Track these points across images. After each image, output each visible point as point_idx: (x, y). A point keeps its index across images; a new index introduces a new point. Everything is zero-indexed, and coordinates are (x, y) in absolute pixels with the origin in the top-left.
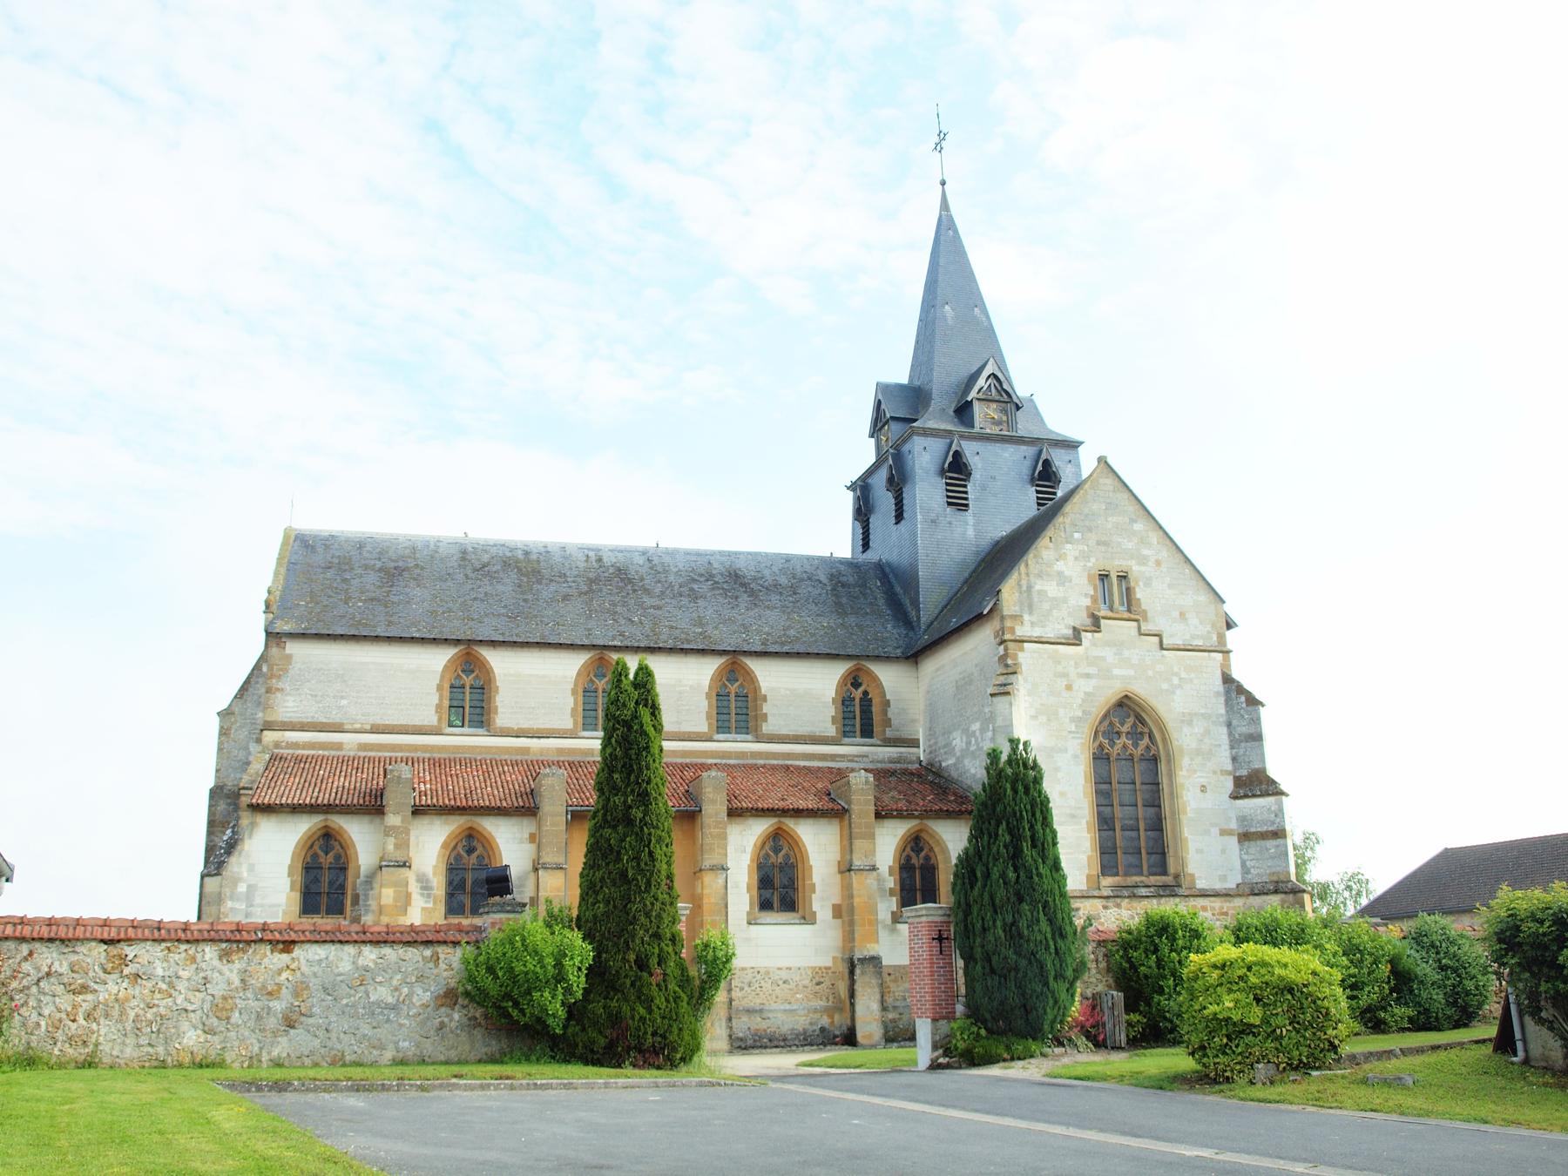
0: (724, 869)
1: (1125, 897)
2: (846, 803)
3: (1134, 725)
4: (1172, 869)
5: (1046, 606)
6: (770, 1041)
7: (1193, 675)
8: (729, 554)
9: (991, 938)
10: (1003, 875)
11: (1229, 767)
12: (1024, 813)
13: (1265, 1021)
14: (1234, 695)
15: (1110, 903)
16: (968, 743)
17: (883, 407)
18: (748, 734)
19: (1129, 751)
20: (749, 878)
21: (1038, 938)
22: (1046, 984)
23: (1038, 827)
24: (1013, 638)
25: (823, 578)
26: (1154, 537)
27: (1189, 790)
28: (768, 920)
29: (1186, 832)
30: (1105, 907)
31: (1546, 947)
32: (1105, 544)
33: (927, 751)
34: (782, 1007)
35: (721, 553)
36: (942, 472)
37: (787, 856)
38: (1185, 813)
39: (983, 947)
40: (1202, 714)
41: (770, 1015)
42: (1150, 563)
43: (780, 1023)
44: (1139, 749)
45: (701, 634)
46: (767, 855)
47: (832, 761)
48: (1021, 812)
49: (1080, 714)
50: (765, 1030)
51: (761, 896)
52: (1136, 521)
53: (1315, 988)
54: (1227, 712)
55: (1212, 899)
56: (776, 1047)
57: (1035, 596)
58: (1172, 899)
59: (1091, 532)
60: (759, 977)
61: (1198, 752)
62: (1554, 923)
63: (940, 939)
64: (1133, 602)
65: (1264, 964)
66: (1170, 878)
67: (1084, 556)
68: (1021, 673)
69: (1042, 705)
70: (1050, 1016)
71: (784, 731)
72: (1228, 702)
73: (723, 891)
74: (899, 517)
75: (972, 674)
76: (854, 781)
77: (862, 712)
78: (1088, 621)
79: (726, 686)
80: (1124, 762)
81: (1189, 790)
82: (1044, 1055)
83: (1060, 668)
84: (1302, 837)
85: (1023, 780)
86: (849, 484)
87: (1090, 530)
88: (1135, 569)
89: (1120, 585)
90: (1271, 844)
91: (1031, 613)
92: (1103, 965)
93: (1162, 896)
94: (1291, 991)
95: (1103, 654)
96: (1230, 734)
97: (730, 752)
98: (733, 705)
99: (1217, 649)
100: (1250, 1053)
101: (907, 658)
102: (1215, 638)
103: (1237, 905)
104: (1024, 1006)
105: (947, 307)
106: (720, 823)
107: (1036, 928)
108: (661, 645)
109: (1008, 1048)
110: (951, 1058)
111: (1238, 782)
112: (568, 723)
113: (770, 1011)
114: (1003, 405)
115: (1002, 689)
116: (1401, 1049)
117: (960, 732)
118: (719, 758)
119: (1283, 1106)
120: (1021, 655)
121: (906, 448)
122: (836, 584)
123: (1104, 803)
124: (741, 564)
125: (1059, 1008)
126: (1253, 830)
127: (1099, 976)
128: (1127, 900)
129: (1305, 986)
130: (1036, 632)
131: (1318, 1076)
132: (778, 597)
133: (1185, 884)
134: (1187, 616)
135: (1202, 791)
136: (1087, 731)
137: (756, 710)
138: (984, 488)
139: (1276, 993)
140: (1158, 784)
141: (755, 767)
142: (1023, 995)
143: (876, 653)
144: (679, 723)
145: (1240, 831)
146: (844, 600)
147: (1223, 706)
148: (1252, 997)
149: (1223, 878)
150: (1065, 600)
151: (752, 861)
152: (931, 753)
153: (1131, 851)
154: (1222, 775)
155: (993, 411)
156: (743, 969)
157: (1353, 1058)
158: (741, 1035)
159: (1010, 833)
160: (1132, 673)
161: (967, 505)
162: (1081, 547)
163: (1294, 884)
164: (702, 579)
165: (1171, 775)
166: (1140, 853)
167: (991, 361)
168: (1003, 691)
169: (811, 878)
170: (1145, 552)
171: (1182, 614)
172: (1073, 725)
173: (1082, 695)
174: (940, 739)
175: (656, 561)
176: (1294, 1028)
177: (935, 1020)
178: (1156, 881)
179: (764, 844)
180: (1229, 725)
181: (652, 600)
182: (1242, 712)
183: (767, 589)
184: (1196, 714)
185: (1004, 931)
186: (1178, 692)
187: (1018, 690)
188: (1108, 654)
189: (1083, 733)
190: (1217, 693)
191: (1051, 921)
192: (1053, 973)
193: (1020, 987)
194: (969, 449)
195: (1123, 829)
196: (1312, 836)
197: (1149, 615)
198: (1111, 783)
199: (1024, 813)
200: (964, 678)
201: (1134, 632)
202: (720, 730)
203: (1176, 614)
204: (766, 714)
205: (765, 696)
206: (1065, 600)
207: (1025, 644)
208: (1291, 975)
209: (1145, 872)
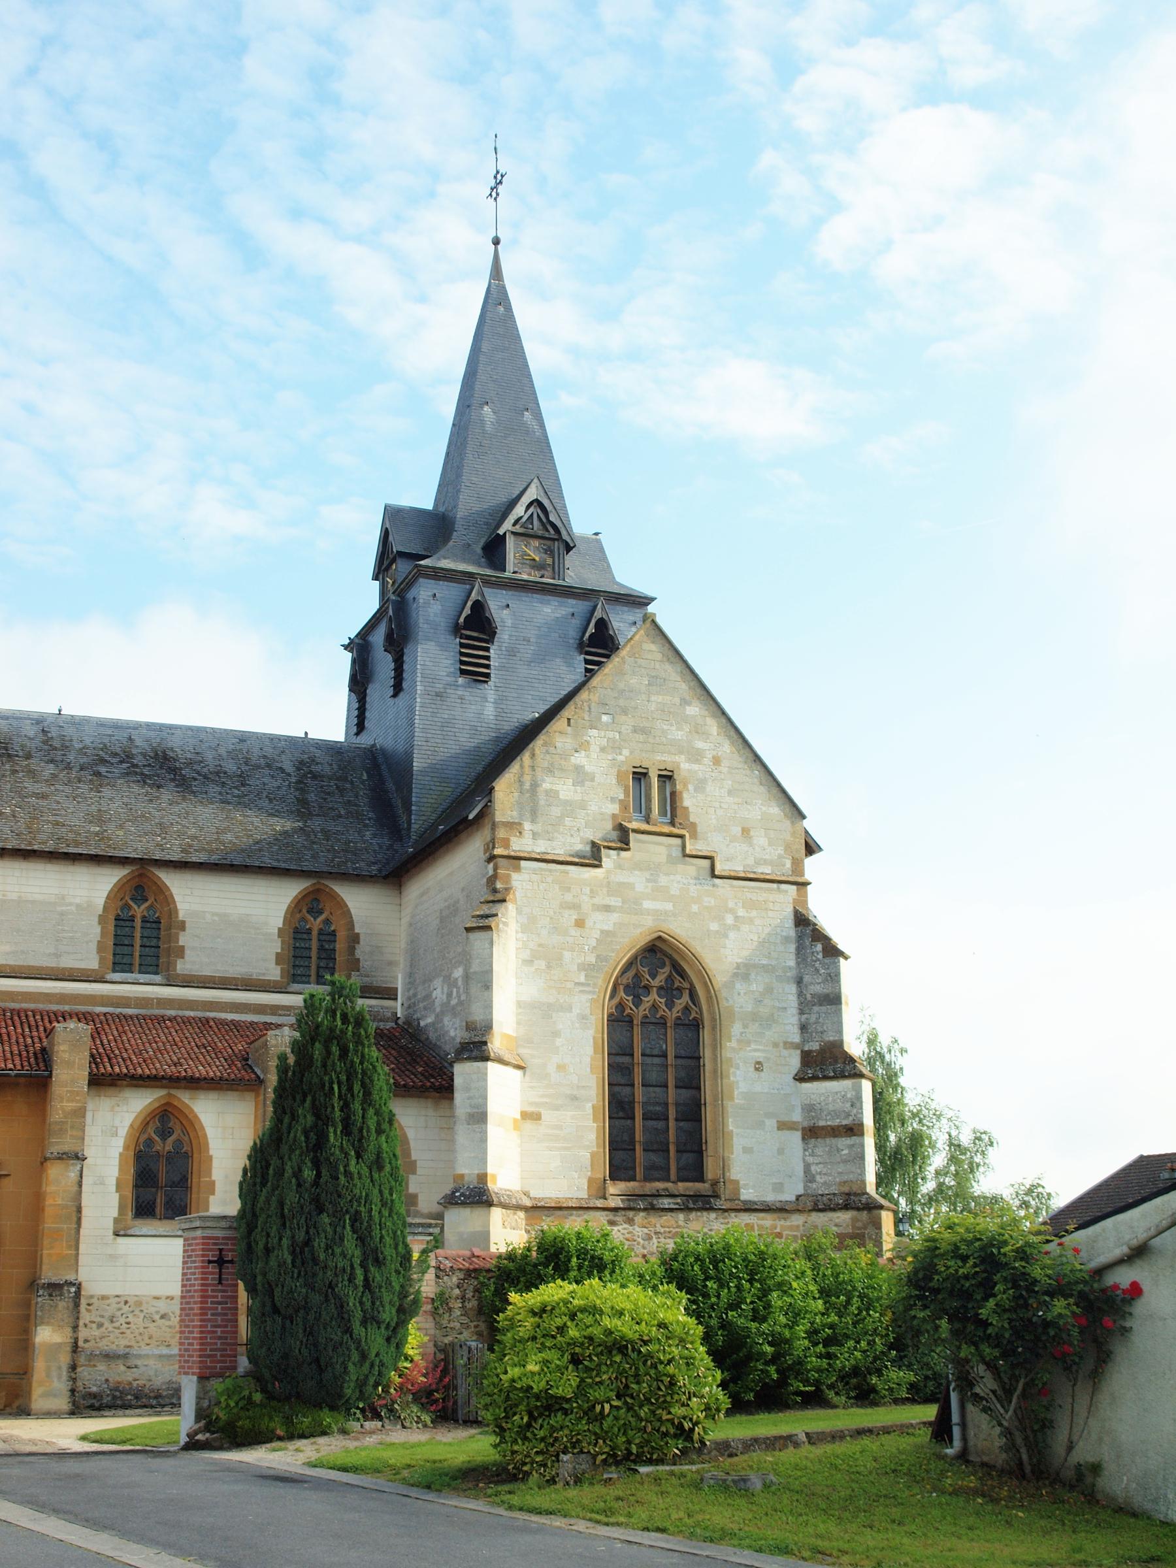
0: (77, 1158)
1: (640, 1210)
2: (263, 1071)
3: (670, 978)
4: (710, 1172)
5: (556, 811)
6: (137, 1398)
7: (754, 913)
8: (161, 727)
9: (273, 1263)
10: (298, 1173)
11: (796, 1038)
12: (336, 1087)
13: (581, 1390)
14: (807, 942)
15: (619, 1218)
16: (450, 995)
17: (391, 538)
18: (156, 973)
19: (661, 1013)
20: (121, 1170)
21: (340, 1265)
22: (348, 1330)
23: (357, 1106)
24: (505, 853)
25: (288, 767)
26: (713, 726)
27: (738, 1068)
28: (144, 1231)
29: (731, 1125)
30: (612, 1223)
31: (967, 1295)
32: (644, 731)
33: (405, 1005)
34: (157, 1352)
35: (149, 726)
36: (456, 630)
37: (178, 1142)
38: (732, 1099)
39: (264, 1274)
40: (764, 966)
41: (139, 1363)
42: (706, 761)
43: (152, 1373)
44: (675, 1010)
45: (97, 834)
46: (150, 1139)
47: (272, 1014)
48: (331, 1083)
49: (593, 960)
50: (130, 1383)
51: (137, 1198)
52: (689, 704)
53: (657, 1347)
54: (798, 964)
55: (762, 1215)
56: (145, 1406)
57: (542, 797)
58: (705, 1214)
59: (626, 714)
60: (126, 1308)
61: (755, 1017)
62: (983, 1260)
63: (221, 1262)
64: (679, 812)
65: (593, 1311)
66: (707, 1185)
67: (614, 747)
68: (515, 901)
69: (540, 945)
70: (353, 1373)
71: (207, 972)
72: (800, 950)
73: (76, 1188)
74: (398, 688)
75: (458, 901)
76: (273, 1042)
77: (321, 948)
78: (615, 835)
79: (130, 907)
80: (652, 1027)
81: (738, 1068)
82: (344, 1432)
83: (569, 897)
84: (972, 1137)
85: (339, 1039)
86: (347, 642)
87: (625, 711)
88: (684, 767)
89: (662, 789)
90: (843, 1142)
91: (533, 821)
92: (472, 1304)
93: (691, 1210)
94: (622, 1350)
95: (631, 880)
96: (800, 994)
97: (128, 998)
98: (138, 934)
99: (791, 879)
100: (556, 1439)
101: (385, 877)
102: (788, 864)
103: (795, 1223)
104: (317, 1360)
105: (486, 408)
106: (78, 1093)
107: (338, 1251)
108: (36, 847)
109: (288, 1421)
110: (213, 1433)
111: (808, 1059)
112: (91, 962)
113: (139, 1356)
114: (549, 543)
115: (482, 923)
116: (807, 1434)
117: (441, 979)
118: (112, 1005)
119: (558, 1522)
120: (515, 876)
121: (410, 595)
122: (305, 776)
123: (623, 1082)
124: (175, 742)
125: (372, 1365)
126: (822, 1123)
127: (465, 1320)
128: (642, 1214)
129: (645, 1343)
130: (540, 847)
131: (648, 1475)
132: (219, 789)
133: (725, 1193)
134: (752, 833)
135: (757, 1069)
136: (602, 984)
137: (169, 942)
138: (512, 652)
139: (602, 1353)
140: (699, 1058)
141: (161, 1019)
142: (315, 1345)
143: (343, 869)
144: (57, 955)
145: (806, 1124)
146: (312, 797)
147: (793, 957)
148: (567, 1357)
149: (778, 1188)
150: (583, 805)
151: (126, 1148)
152: (409, 1007)
153: (655, 1147)
154: (786, 1048)
155: (533, 550)
156: (104, 1298)
157: (725, 1448)
158: (94, 1389)
159: (317, 1116)
160: (669, 906)
161: (488, 675)
162: (610, 734)
163: (870, 1197)
164: (114, 760)
165: (716, 1046)
166: (668, 1151)
167: (533, 486)
168: (483, 925)
169: (209, 1174)
170: (700, 745)
171: (745, 831)
172: (583, 973)
173: (597, 934)
174: (420, 988)
175: (54, 733)
176: (626, 1403)
177: (202, 1378)
178: (687, 1189)
179: (145, 1125)
180: (799, 982)
181: (37, 786)
182: (817, 964)
183: (205, 777)
184: (755, 966)
185: (293, 1253)
186: (732, 935)
187: (505, 924)
188: (639, 881)
189: (595, 985)
190: (786, 939)
191: (362, 1240)
192: (359, 1314)
193: (311, 1333)
194: (498, 605)
195: (646, 1117)
196: (983, 1136)
197: (699, 829)
198: (632, 1055)
199: (336, 1087)
200: (448, 907)
201: (677, 852)
202: (143, 968)
203: (737, 830)
204: (183, 947)
205: (183, 922)
206: (583, 805)
207: (523, 863)
208: (624, 1328)
209: (673, 1176)
